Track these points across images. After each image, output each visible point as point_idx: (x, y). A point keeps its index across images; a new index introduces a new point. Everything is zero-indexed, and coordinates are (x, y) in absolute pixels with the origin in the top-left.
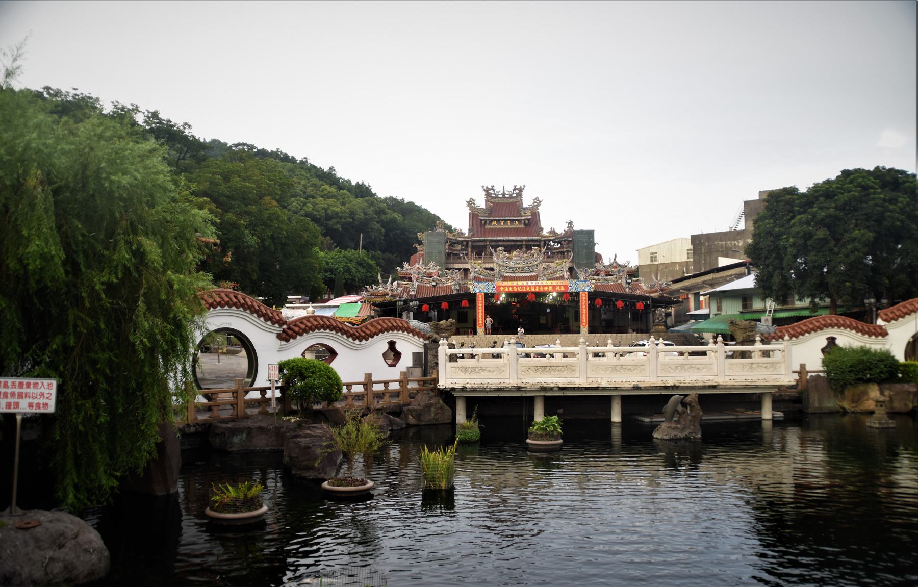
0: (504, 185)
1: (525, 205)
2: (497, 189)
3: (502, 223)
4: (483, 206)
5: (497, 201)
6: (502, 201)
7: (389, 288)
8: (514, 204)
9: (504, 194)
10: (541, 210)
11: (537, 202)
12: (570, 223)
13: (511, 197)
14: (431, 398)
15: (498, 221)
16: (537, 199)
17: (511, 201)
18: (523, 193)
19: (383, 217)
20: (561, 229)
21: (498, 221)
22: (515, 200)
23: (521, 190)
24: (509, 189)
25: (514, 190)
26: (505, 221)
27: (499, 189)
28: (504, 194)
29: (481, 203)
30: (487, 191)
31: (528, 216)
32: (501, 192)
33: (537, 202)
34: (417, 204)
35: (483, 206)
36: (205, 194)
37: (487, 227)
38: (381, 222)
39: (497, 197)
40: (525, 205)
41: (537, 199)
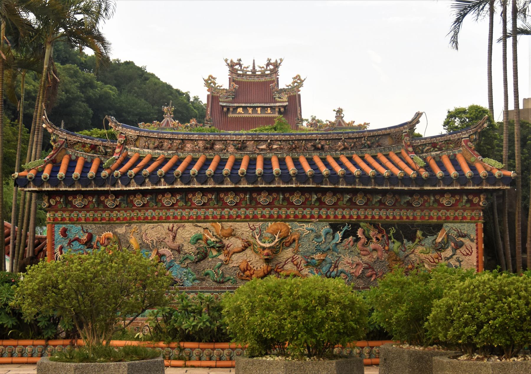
0: (254, 59)
1: (282, 86)
2: (245, 64)
3: (250, 111)
4: (226, 86)
5: (244, 79)
6: (251, 80)
7: (41, 105)
8: (266, 84)
9: (254, 71)
10: (303, 92)
11: (299, 82)
12: (339, 112)
13: (263, 75)
14: (114, 200)
15: (245, 108)
16: (298, 77)
17: (263, 80)
18: (280, 69)
19: (91, 92)
20: (327, 116)
21: (245, 108)
22: (268, 79)
23: (276, 66)
24: (261, 63)
25: (268, 65)
26: (254, 108)
27: (247, 63)
28: (254, 71)
29: (223, 82)
30: (232, 65)
31: (284, 101)
32: (251, 68)
33: (299, 82)
34: (138, 64)
35: (226, 86)
36: (197, 279)
37: (230, 115)
38: (88, 100)
39: (245, 75)
40: (282, 86)
41: (298, 77)
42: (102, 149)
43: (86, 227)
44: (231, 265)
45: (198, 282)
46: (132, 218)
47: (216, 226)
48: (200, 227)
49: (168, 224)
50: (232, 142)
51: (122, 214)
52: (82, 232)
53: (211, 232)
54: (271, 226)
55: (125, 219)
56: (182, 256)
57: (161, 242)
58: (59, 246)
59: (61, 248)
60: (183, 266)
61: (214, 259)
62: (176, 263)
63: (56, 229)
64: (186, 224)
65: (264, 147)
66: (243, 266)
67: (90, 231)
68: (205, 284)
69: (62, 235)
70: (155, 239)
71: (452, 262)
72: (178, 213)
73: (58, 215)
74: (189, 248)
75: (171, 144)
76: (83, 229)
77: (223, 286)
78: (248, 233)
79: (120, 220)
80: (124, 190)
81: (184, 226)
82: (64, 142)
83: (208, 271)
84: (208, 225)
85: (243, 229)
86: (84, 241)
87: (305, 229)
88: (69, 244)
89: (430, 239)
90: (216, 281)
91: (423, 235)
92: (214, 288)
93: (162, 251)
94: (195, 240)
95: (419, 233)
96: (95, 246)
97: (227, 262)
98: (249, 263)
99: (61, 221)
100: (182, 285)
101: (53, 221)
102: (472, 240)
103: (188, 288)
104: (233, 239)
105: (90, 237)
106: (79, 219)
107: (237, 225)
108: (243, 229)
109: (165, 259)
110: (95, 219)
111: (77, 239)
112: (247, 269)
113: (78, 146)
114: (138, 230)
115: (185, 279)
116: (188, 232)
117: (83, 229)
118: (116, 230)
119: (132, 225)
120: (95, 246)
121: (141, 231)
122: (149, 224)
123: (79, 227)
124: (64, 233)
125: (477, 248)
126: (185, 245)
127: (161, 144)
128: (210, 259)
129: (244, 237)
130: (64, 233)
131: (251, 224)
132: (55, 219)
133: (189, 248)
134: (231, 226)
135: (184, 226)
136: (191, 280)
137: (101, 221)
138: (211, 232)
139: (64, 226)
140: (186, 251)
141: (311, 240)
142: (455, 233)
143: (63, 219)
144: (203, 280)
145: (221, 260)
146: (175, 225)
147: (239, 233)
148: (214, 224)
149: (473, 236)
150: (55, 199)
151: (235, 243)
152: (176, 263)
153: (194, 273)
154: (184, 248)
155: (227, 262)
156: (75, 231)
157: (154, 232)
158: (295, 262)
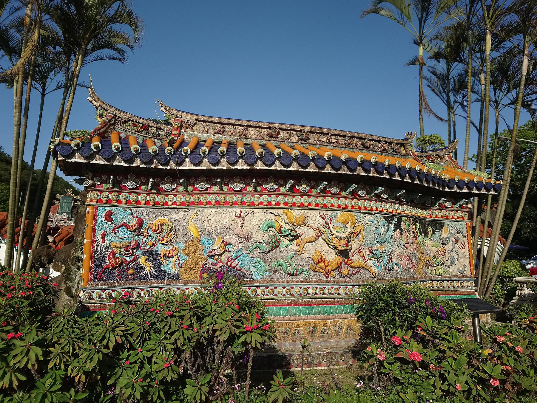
42: (155, 130)
43: (136, 211)
44: (303, 256)
45: (268, 274)
46: (192, 203)
47: (288, 213)
48: (272, 213)
49: (235, 210)
50: (295, 133)
51: (179, 199)
52: (131, 216)
53: (283, 219)
54: (341, 216)
55: (183, 203)
56: (250, 244)
57: (227, 228)
58: (102, 232)
59: (104, 235)
60: (252, 256)
61: (286, 248)
62: (245, 253)
63: (98, 212)
64: (255, 210)
65: (324, 140)
66: (317, 258)
67: (140, 216)
68: (277, 276)
69: (106, 219)
70: (219, 226)
71: (453, 254)
72: (247, 199)
73: (103, 196)
74: (260, 236)
75: (234, 130)
76: (132, 213)
77: (295, 278)
78: (319, 222)
79: (176, 205)
80: (192, 170)
81: (253, 213)
82: (113, 117)
83: (281, 261)
84: (280, 212)
85: (314, 218)
86: (134, 228)
87: (366, 221)
88: (114, 230)
89: (437, 234)
90: (289, 274)
91: (434, 231)
92: (287, 282)
93: (227, 239)
94: (267, 227)
95: (430, 229)
96: (146, 233)
97: (298, 253)
98: (322, 254)
99: (106, 203)
100: (251, 278)
101: (97, 202)
102: (464, 237)
103: (258, 282)
104: (304, 227)
105: (141, 223)
106: (128, 202)
107: (307, 213)
108: (314, 218)
109: (231, 249)
110: (147, 203)
111: (125, 225)
112: (322, 260)
113: (128, 124)
114: (199, 216)
115: (255, 270)
116: (258, 218)
117: (132, 213)
118: (171, 216)
119: (192, 210)
120: (146, 233)
121: (202, 217)
122: (212, 210)
123: (128, 210)
124: (109, 217)
125: (468, 243)
126: (254, 233)
127: (222, 130)
128: (282, 249)
129: (315, 226)
130: (109, 217)
131: (322, 212)
132: (99, 201)
133: (260, 236)
134: (303, 214)
135: (253, 213)
136: (262, 272)
137: (154, 205)
138: (283, 219)
139: (109, 209)
140: (255, 239)
141: (372, 231)
142: (454, 230)
143: (109, 201)
144: (275, 271)
145: (294, 250)
146: (244, 211)
147: (310, 222)
148: (286, 211)
149: (465, 233)
150: (101, 177)
151: (306, 232)
152: (245, 253)
153: (264, 264)
154: (253, 236)
155: (298, 253)
156: (122, 215)
157: (217, 218)
158: (361, 254)
